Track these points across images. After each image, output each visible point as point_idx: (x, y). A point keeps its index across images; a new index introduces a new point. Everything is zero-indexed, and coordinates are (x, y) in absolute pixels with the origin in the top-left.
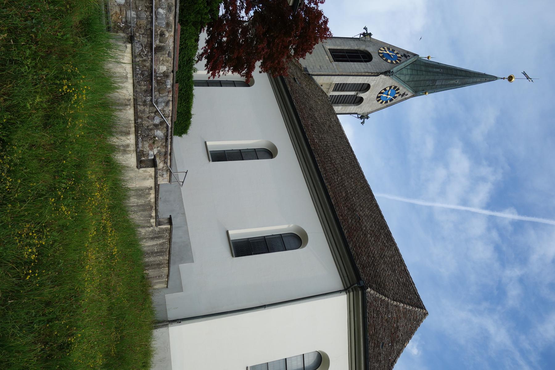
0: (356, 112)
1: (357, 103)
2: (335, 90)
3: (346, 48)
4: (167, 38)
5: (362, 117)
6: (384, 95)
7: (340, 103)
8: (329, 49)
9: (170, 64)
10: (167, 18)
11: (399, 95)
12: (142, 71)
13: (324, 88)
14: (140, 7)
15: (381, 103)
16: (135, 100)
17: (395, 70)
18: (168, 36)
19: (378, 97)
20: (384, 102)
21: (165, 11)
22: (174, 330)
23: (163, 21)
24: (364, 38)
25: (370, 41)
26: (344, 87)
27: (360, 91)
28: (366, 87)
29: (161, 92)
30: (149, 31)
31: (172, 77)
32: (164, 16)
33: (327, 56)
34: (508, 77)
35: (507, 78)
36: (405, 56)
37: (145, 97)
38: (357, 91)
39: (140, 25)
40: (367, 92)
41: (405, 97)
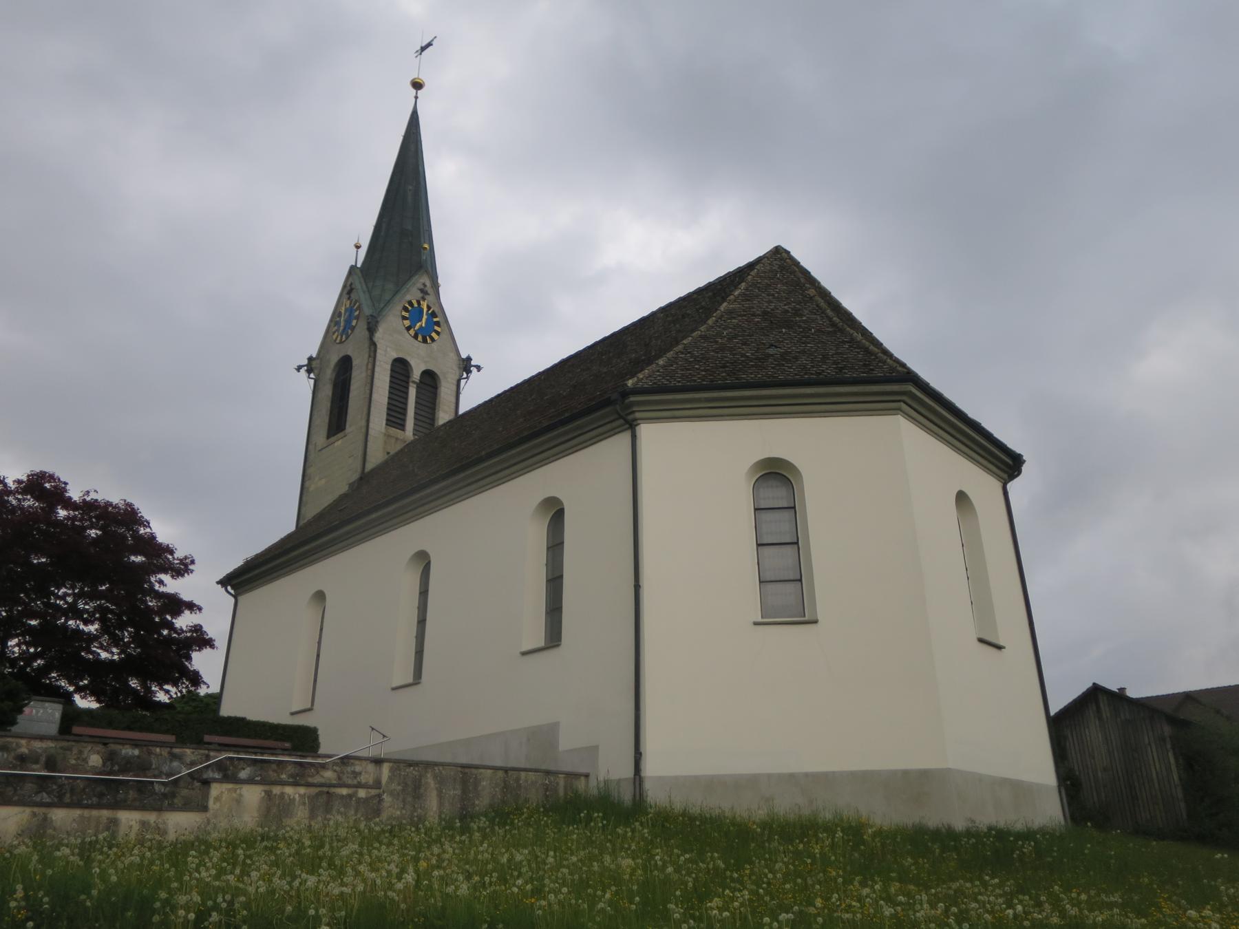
0: (455, 382)
2: (402, 427)
13: (395, 448)
15: (438, 333)
19: (425, 341)
20: (436, 328)
22: (651, 768)
24: (316, 371)
28: (400, 367)
33: (336, 444)
35: (415, 91)
36: (349, 293)
38: (408, 383)
41: (429, 289)
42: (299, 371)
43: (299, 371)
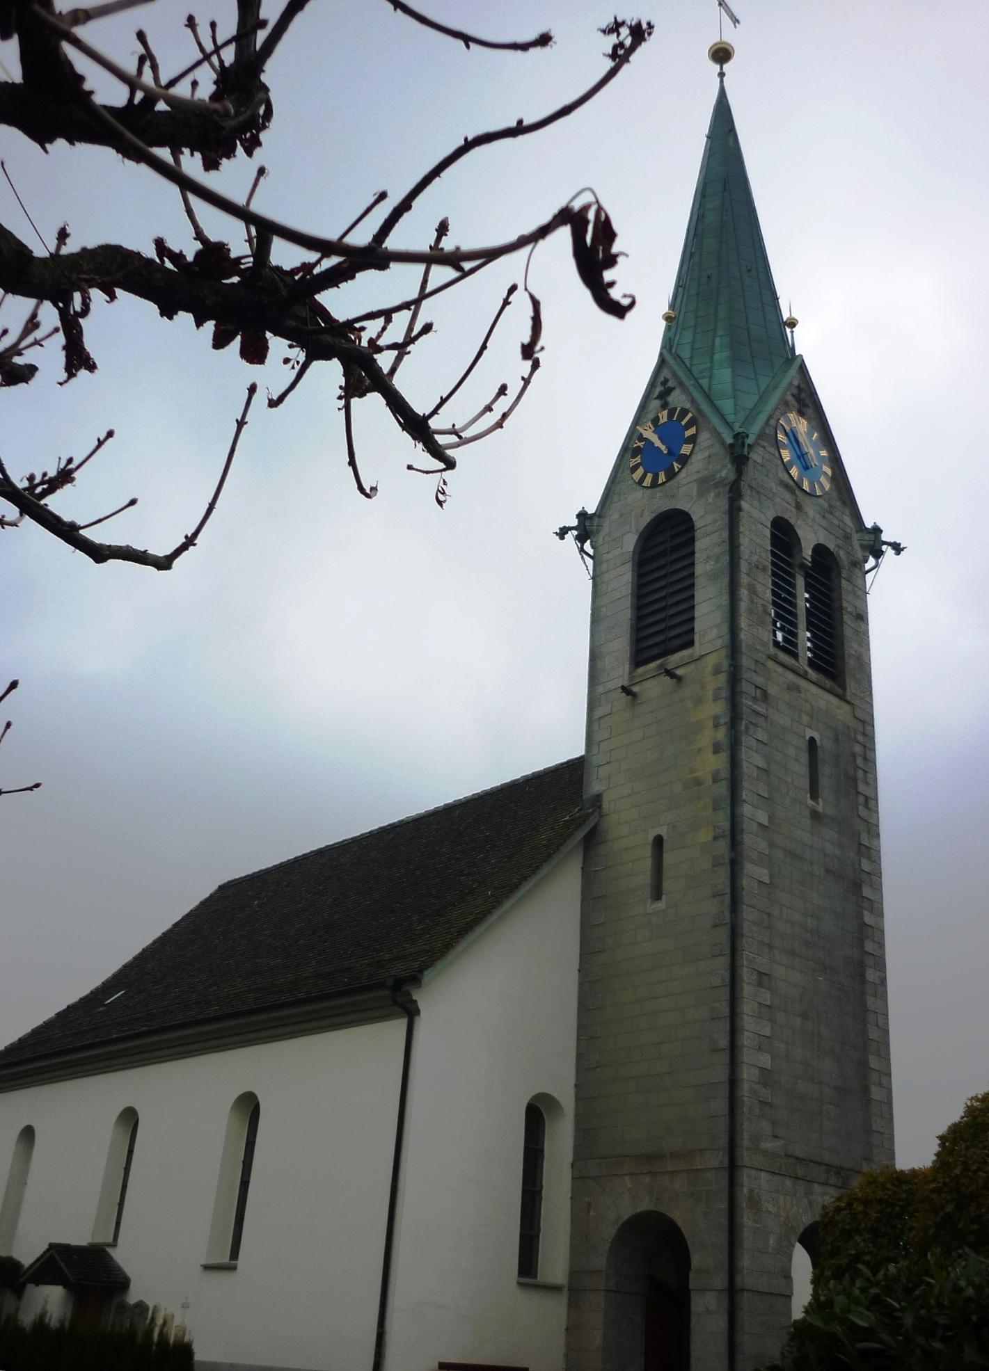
42: (562, 538)
43: (562, 538)
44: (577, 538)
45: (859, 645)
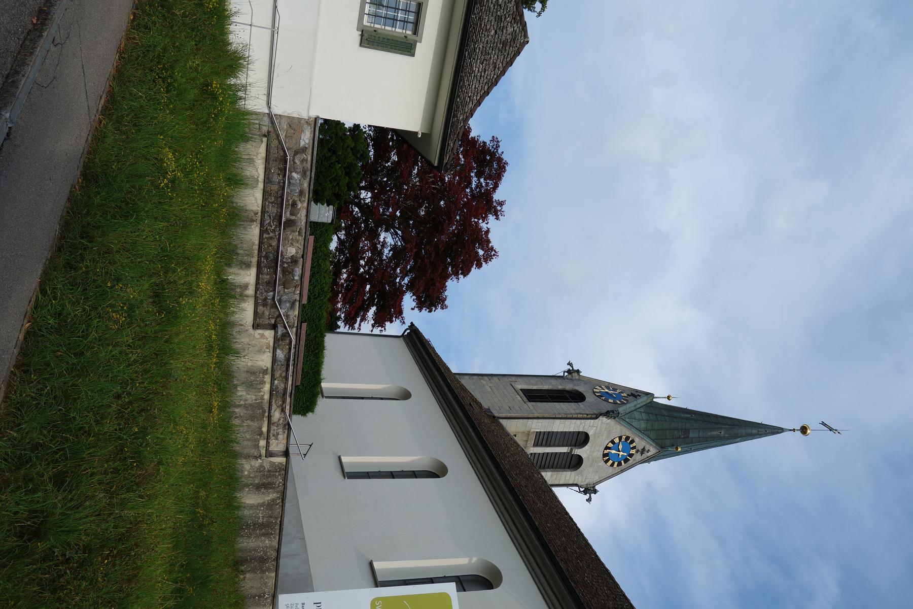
0: (575, 483)
1: (573, 467)
2: (536, 445)
3: (546, 387)
4: (299, 209)
5: (586, 492)
6: (613, 452)
7: (548, 468)
8: (521, 390)
9: (301, 244)
10: (301, 184)
11: (637, 452)
12: (266, 253)
13: (520, 440)
14: (273, 169)
15: (612, 465)
16: (263, 212)
17: (621, 409)
18: (301, 208)
19: (605, 455)
20: (616, 463)
21: (299, 176)
23: (296, 188)
25: (579, 380)
26: (549, 440)
27: (575, 446)
28: (582, 439)
29: (287, 286)
30: (280, 199)
31: (302, 264)
32: (298, 181)
34: (801, 428)
37: (267, 292)
38: (570, 446)
39: (271, 190)
40: (586, 447)
44: (569, 370)
45: (377, 326)
